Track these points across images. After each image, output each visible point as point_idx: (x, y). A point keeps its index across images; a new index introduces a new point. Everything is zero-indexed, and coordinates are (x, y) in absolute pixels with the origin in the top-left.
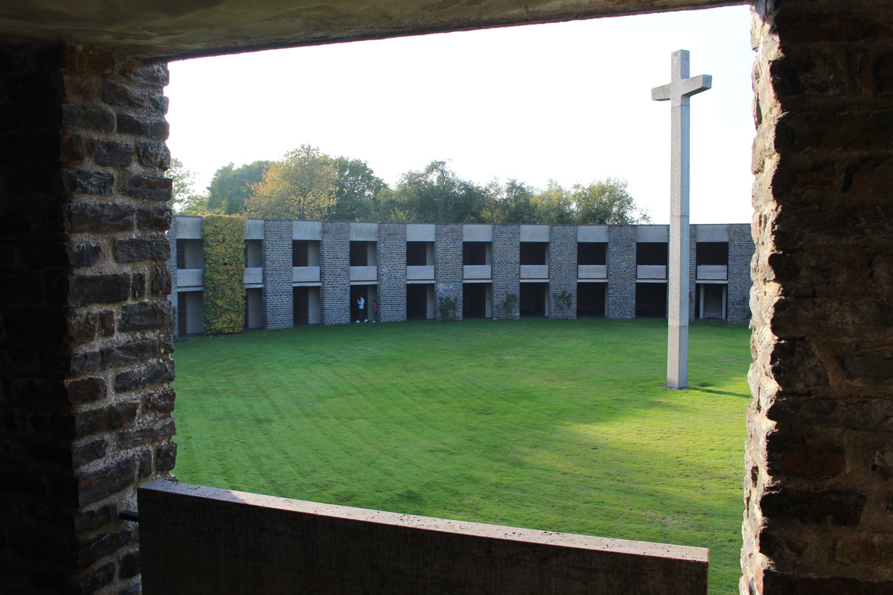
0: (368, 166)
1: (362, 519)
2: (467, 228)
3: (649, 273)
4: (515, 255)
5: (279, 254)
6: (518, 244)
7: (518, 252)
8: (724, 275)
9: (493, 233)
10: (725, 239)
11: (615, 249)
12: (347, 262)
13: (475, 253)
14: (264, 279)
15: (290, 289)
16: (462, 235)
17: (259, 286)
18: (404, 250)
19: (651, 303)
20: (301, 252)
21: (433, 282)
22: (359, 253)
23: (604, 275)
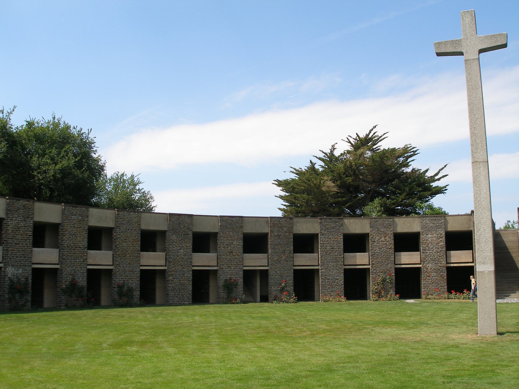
0: (304, 166)
1: (500, 44)
2: (346, 221)
3: (459, 258)
4: (239, 244)
6: (87, 227)
7: (86, 236)
11: (174, 237)
16: (33, 214)
19: (460, 280)
23: (163, 262)
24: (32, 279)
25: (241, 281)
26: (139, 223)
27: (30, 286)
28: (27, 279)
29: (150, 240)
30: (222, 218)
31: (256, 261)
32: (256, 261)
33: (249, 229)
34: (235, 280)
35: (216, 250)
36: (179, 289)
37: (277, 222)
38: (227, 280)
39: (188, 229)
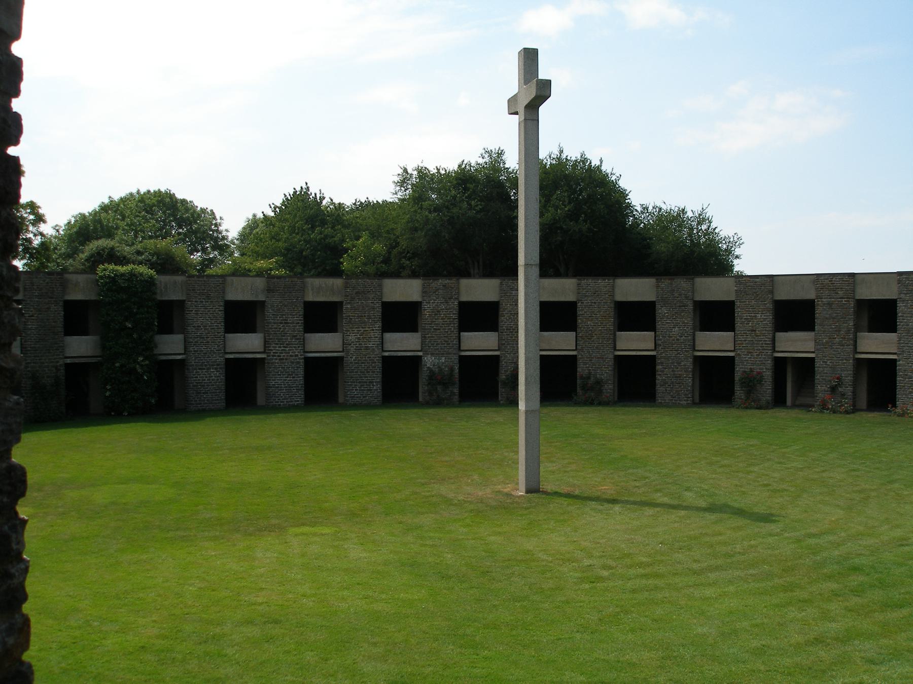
3: (480, 342)
5: (205, 317)
8: (811, 346)
9: (501, 290)
10: (811, 295)
12: (300, 327)
13: (635, 316)
14: (185, 348)
15: (221, 360)
16: (458, 293)
17: (258, 356)
18: (378, 312)
20: (242, 316)
21: (420, 354)
22: (322, 317)
23: (651, 346)
24: (460, 368)
25: (768, 375)
26: (612, 293)
27: (457, 376)
28: (452, 369)
29: (716, 315)
30: (818, 278)
31: (796, 344)
32: (796, 344)
33: (782, 294)
34: (759, 373)
35: (183, 330)
36: (672, 383)
37: (827, 281)
38: (745, 372)
39: (687, 298)
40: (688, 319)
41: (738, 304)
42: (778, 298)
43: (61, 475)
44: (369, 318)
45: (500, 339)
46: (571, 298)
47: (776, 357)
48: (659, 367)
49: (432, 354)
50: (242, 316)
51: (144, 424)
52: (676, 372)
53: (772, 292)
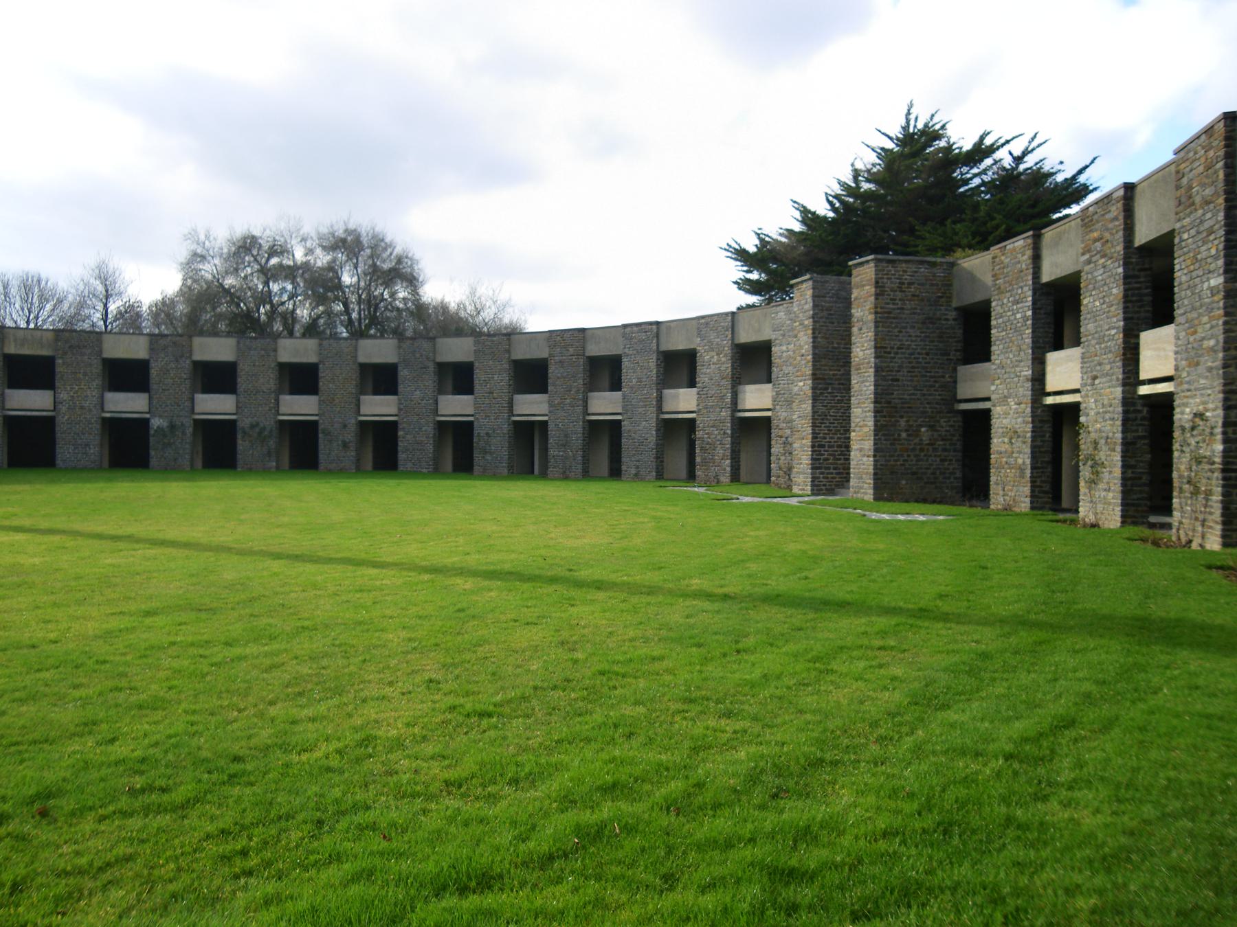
16: (191, 352)
21: (148, 416)
40: (429, 381)
41: (476, 364)
42: (514, 357)
43: (922, 518)
44: (85, 374)
45: (238, 402)
46: (312, 359)
47: (439, 422)
48: (400, 433)
49: (160, 417)
50: (302, 378)
51: (176, 480)
52: (416, 438)
53: (508, 351)
